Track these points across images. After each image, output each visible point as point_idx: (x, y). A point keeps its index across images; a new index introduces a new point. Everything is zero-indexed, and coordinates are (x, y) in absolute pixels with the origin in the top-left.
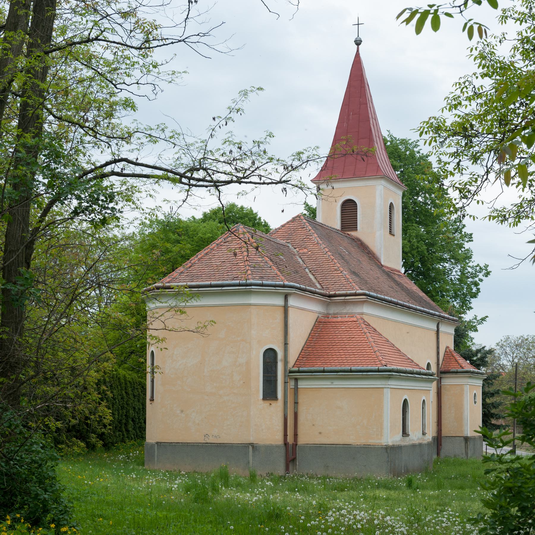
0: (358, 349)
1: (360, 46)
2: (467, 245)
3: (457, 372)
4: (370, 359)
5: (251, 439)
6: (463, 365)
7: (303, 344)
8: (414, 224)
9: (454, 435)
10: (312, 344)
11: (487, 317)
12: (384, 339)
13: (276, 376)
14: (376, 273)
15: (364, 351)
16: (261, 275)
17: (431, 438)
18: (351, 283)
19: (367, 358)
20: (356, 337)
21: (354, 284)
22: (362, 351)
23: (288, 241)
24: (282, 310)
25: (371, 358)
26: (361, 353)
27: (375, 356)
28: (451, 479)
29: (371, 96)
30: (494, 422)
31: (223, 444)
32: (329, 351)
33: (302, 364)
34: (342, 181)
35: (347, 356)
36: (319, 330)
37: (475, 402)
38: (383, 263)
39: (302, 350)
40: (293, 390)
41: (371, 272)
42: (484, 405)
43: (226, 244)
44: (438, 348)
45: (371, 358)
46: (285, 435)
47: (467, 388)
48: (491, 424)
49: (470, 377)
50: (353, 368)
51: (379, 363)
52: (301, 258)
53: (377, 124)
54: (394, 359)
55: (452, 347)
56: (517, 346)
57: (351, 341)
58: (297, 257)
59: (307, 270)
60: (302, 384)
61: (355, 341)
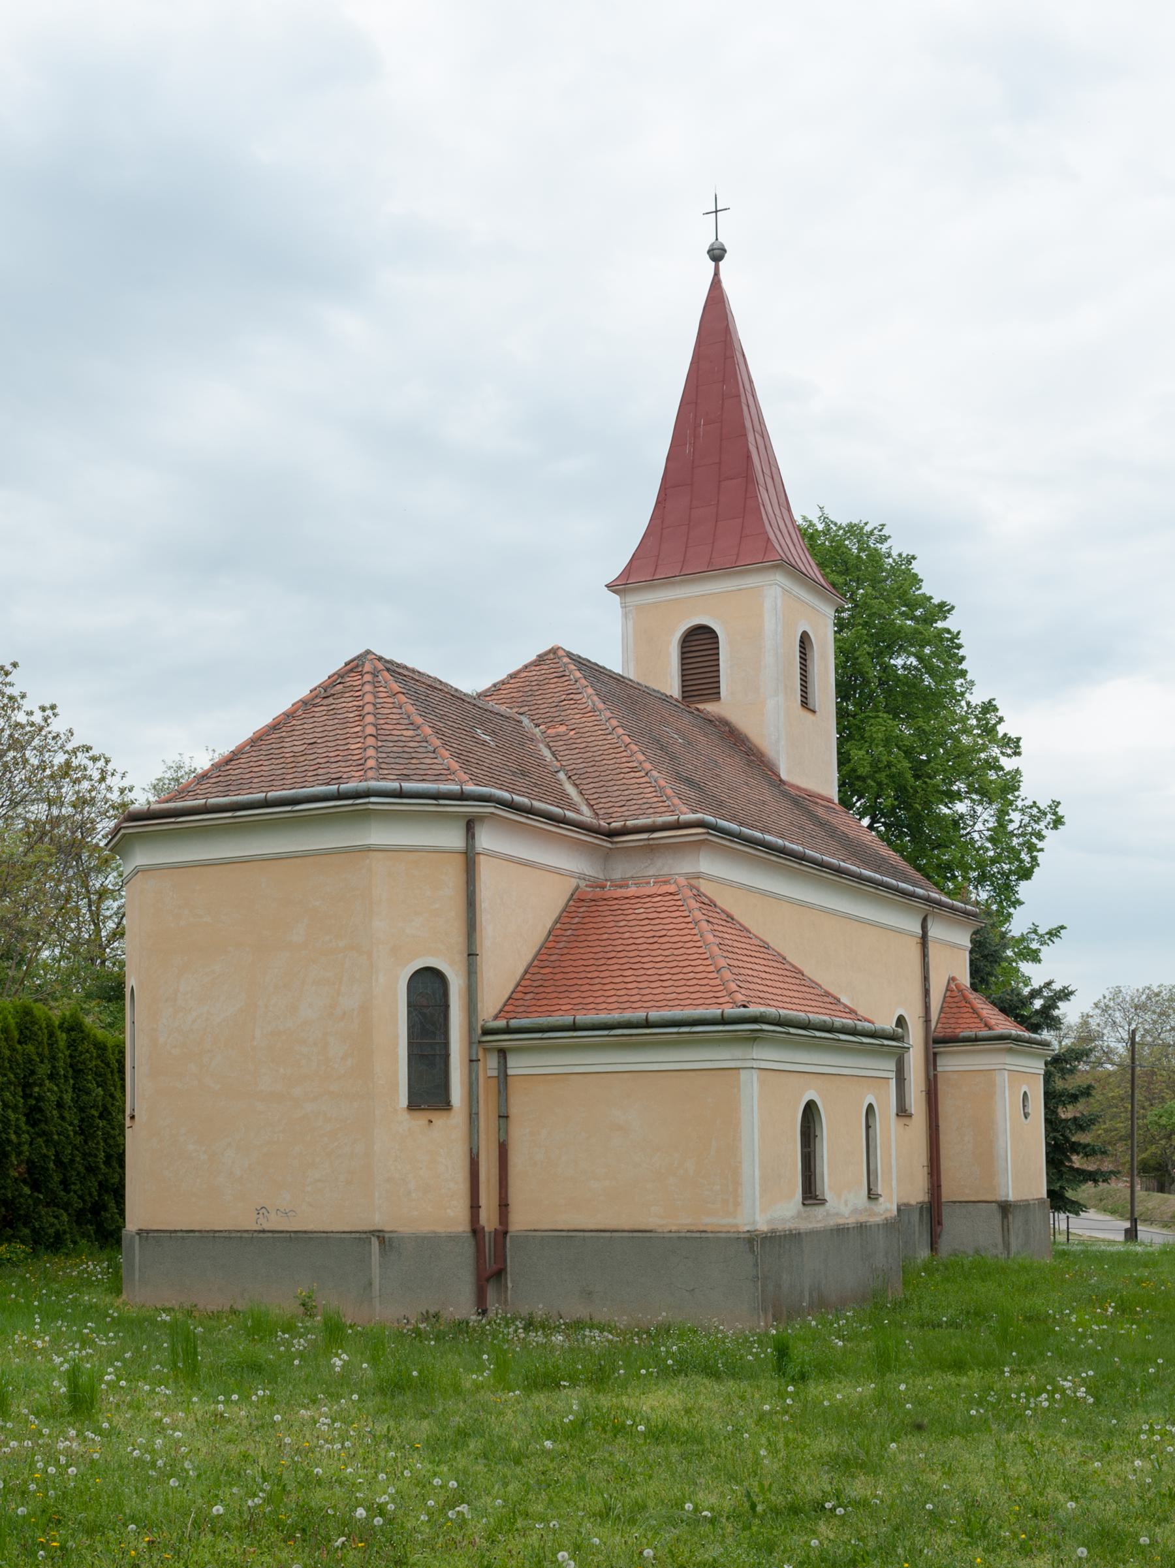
0: (675, 964)
1: (721, 263)
2: (1008, 764)
3: (976, 1040)
4: (703, 989)
5: (378, 1219)
6: (993, 1022)
7: (529, 957)
8: (881, 714)
9: (973, 1199)
10: (553, 958)
11: (1062, 927)
12: (758, 942)
13: (446, 1045)
14: (768, 794)
15: (689, 969)
16: (405, 772)
17: (895, 1208)
18: (668, 798)
19: (697, 988)
20: (670, 933)
21: (676, 801)
22: (685, 970)
23: (522, 710)
24: (459, 862)
25: (707, 988)
26: (681, 976)
27: (718, 982)
28: (940, 1326)
29: (751, 382)
30: (1077, 1161)
31: (305, 1232)
32: (595, 974)
33: (521, 1009)
34: (682, 581)
35: (641, 985)
36: (576, 920)
37: (1026, 1115)
38: (784, 776)
39: (526, 972)
40: (496, 1080)
41: (745, 789)
42: (1052, 1123)
43: (325, 702)
44: (926, 979)
45: (707, 988)
46: (475, 1207)
47: (1003, 1079)
48: (1071, 1168)
49: (1010, 1050)
50: (654, 1015)
51: (727, 999)
52: (550, 748)
53: (768, 447)
54: (779, 991)
55: (965, 980)
56: (1136, 1007)
57: (656, 946)
58: (541, 746)
59: (562, 776)
60: (518, 1065)
61: (669, 946)
